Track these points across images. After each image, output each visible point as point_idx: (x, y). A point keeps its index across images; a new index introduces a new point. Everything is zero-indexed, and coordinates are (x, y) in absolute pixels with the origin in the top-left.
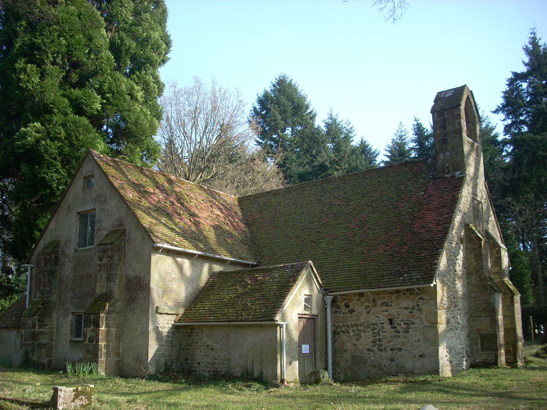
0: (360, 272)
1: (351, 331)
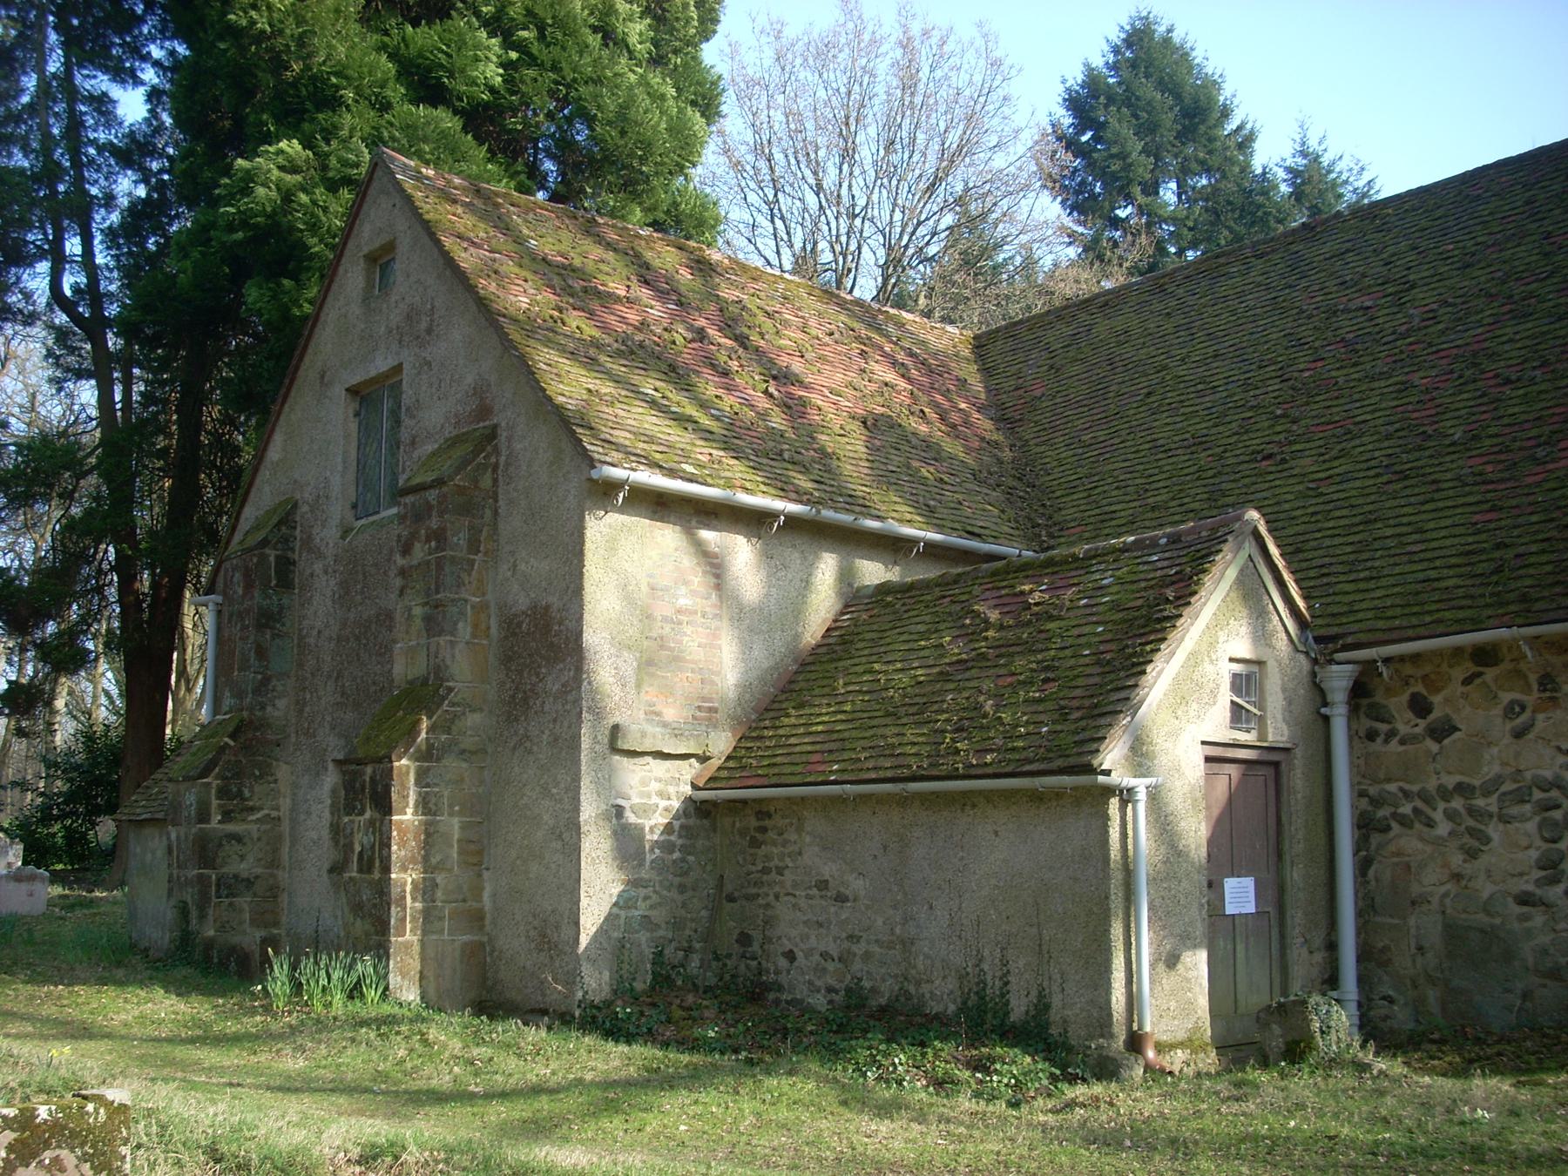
0: (1475, 558)
1: (1438, 816)
